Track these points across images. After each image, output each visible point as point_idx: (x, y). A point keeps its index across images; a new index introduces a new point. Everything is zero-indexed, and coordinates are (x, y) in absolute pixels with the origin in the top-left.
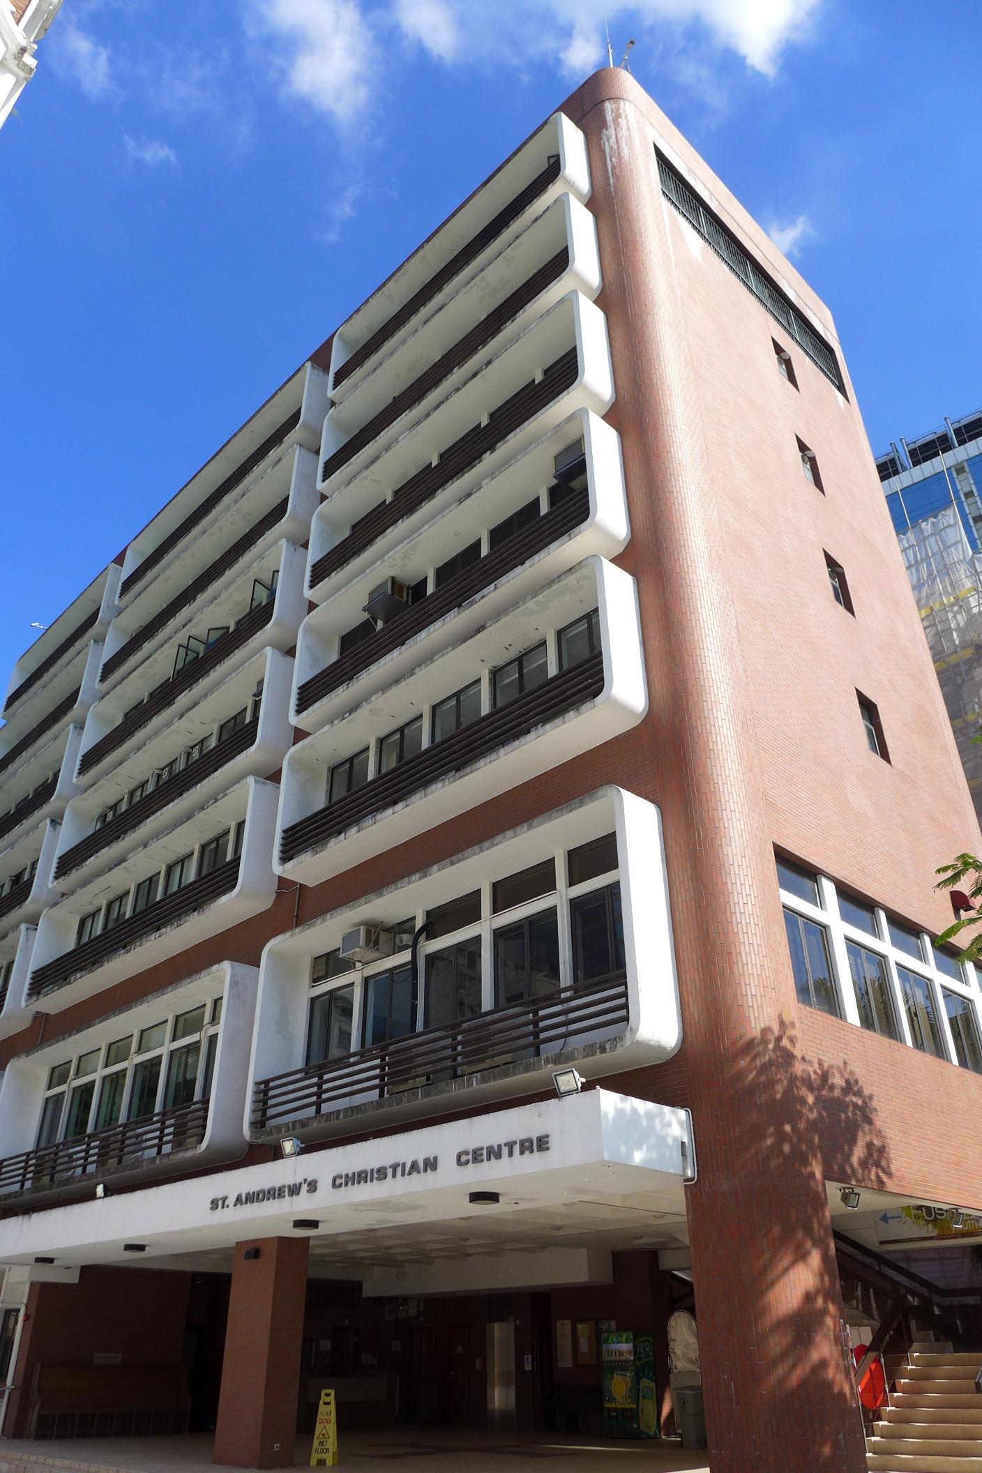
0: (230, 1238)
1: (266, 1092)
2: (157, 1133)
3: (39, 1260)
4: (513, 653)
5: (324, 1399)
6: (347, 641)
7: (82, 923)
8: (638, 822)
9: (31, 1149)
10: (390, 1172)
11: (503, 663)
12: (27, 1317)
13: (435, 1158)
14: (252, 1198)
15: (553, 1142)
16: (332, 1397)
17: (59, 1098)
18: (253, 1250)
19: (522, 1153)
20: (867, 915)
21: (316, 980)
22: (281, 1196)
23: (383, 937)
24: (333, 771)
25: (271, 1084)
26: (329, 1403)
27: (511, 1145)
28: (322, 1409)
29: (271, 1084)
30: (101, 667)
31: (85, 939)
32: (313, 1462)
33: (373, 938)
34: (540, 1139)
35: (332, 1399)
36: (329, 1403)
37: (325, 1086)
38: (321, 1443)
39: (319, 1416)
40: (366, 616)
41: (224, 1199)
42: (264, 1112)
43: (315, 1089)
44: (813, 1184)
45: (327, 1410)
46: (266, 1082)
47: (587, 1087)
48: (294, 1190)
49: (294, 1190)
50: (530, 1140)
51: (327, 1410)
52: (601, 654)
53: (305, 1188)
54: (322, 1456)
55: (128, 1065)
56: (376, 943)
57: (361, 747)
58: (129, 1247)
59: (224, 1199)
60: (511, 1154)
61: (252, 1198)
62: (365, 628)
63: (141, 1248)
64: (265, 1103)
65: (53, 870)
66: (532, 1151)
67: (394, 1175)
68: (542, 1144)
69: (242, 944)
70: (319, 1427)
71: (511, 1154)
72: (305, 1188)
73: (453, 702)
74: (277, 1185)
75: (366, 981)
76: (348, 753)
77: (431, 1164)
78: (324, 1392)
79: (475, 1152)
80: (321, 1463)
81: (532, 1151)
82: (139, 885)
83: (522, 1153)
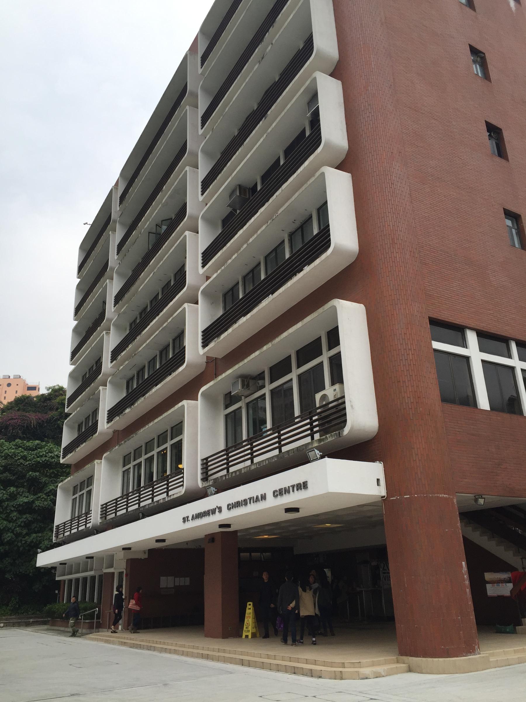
0: (201, 535)
1: (206, 463)
2: (166, 486)
3: (124, 549)
4: (298, 224)
5: (248, 607)
6: (225, 222)
7: (128, 383)
8: (351, 318)
9: (119, 495)
10: (248, 501)
11: (294, 230)
12: (127, 575)
13: (265, 494)
14: (199, 516)
15: (309, 485)
16: (251, 606)
17: (128, 470)
18: (211, 538)
19: (297, 490)
20: (504, 345)
21: (227, 407)
22: (209, 514)
23: (251, 382)
24: (225, 296)
25: (209, 459)
26: (250, 609)
27: (293, 486)
28: (248, 611)
29: (209, 459)
30: (116, 247)
31: (130, 391)
32: (244, 637)
33: (246, 383)
34: (304, 483)
35: (251, 607)
36: (250, 609)
37: (230, 459)
38: (247, 628)
39: (246, 615)
40: (229, 210)
41: (188, 517)
42: (207, 473)
43: (225, 461)
44: (5, 534)
45: (250, 611)
46: (206, 459)
47: (322, 457)
48: (213, 512)
49: (213, 512)
50: (300, 484)
51: (250, 611)
52: (328, 226)
53: (217, 510)
54: (247, 634)
55: (155, 452)
56: (248, 386)
57: (234, 283)
58: (158, 541)
59: (188, 517)
60: (293, 491)
61: (199, 516)
62: (230, 215)
63: (164, 541)
64: (207, 468)
65: (110, 358)
66: (301, 489)
67: (250, 503)
68: (304, 486)
69: (189, 390)
70: (246, 620)
71: (293, 491)
72: (217, 510)
73: (274, 254)
74: (206, 510)
75: (248, 404)
76: (230, 286)
77: (264, 497)
78: (248, 603)
79: (280, 490)
80: (247, 636)
81: (301, 489)
82: (149, 362)
83: (297, 490)
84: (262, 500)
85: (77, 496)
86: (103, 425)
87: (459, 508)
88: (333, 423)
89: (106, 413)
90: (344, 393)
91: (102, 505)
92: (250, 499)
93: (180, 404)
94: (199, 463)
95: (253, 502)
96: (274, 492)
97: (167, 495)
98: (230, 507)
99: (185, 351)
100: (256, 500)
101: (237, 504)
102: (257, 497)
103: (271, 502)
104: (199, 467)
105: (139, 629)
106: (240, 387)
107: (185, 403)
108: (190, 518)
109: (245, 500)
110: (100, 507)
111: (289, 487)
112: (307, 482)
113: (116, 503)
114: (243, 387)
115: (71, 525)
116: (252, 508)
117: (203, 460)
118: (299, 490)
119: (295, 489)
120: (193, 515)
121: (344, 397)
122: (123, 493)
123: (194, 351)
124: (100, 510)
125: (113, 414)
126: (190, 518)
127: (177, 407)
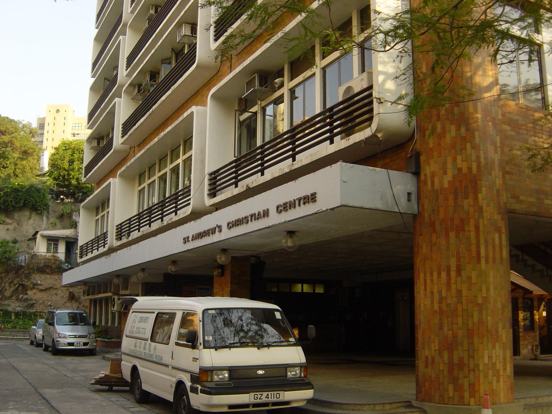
10: (249, 219)
13: (268, 209)
27: (300, 200)
34: (312, 195)
53: (217, 229)
59: (188, 238)
64: (215, 183)
68: (311, 198)
77: (266, 213)
81: (309, 203)
83: (304, 203)
84: (264, 217)
85: (99, 216)
86: (118, 140)
87: (511, 217)
88: (358, 120)
89: (121, 126)
90: (372, 81)
91: (117, 226)
92: (252, 216)
93: (189, 112)
94: (207, 178)
95: (255, 220)
96: (278, 207)
97: (176, 214)
98: (230, 225)
99: (196, 48)
100: (255, 217)
101: (238, 223)
102: (259, 213)
103: (274, 219)
104: (207, 182)
105: (415, 365)
106: (257, 83)
107: (194, 109)
108: (190, 239)
109: (246, 218)
110: (115, 228)
111: (294, 200)
112: (315, 193)
113: (129, 223)
114: (261, 85)
115: (92, 246)
116: (253, 226)
117: (210, 174)
118: (307, 204)
119: (302, 202)
120: (193, 235)
121: (370, 87)
122: (139, 211)
123: (206, 46)
124: (115, 231)
125: (127, 126)
126: (190, 239)
127: (185, 115)
